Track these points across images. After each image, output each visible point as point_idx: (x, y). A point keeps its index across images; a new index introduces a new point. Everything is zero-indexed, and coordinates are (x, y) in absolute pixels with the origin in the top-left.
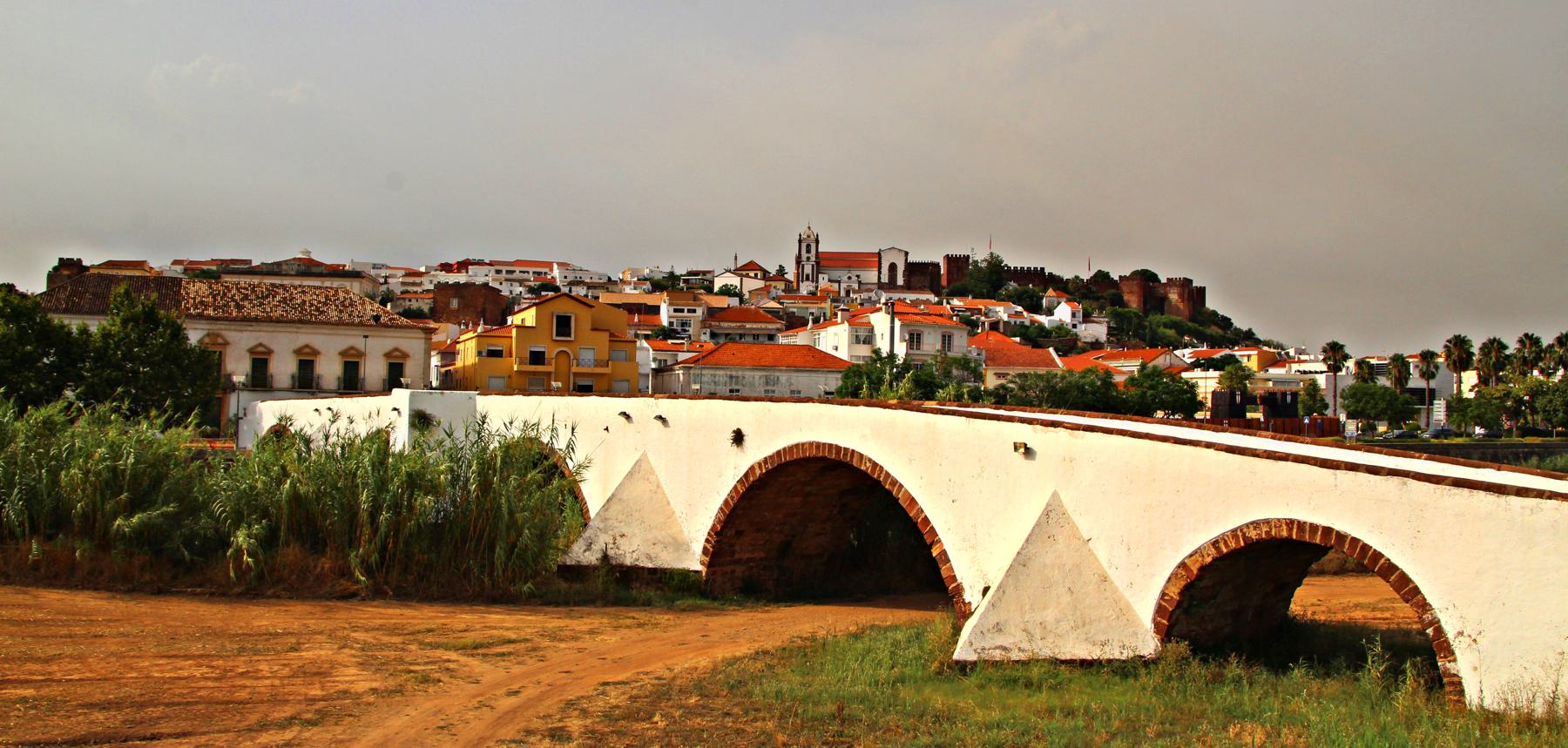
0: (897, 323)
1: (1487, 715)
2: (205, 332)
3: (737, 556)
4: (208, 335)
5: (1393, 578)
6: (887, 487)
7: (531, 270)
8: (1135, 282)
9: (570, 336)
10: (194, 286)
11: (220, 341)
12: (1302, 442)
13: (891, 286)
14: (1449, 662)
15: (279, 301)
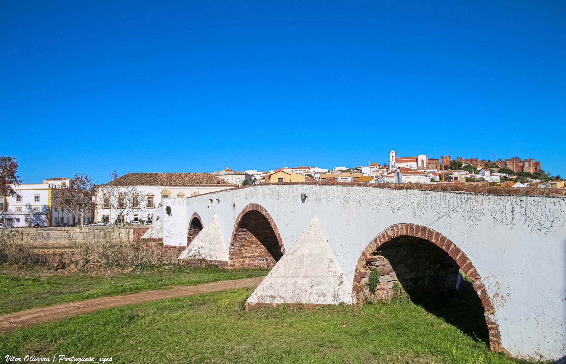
3: (244, 255)
6: (415, 236)
7: (303, 170)
8: (512, 161)
11: (168, 192)
14: (491, 314)
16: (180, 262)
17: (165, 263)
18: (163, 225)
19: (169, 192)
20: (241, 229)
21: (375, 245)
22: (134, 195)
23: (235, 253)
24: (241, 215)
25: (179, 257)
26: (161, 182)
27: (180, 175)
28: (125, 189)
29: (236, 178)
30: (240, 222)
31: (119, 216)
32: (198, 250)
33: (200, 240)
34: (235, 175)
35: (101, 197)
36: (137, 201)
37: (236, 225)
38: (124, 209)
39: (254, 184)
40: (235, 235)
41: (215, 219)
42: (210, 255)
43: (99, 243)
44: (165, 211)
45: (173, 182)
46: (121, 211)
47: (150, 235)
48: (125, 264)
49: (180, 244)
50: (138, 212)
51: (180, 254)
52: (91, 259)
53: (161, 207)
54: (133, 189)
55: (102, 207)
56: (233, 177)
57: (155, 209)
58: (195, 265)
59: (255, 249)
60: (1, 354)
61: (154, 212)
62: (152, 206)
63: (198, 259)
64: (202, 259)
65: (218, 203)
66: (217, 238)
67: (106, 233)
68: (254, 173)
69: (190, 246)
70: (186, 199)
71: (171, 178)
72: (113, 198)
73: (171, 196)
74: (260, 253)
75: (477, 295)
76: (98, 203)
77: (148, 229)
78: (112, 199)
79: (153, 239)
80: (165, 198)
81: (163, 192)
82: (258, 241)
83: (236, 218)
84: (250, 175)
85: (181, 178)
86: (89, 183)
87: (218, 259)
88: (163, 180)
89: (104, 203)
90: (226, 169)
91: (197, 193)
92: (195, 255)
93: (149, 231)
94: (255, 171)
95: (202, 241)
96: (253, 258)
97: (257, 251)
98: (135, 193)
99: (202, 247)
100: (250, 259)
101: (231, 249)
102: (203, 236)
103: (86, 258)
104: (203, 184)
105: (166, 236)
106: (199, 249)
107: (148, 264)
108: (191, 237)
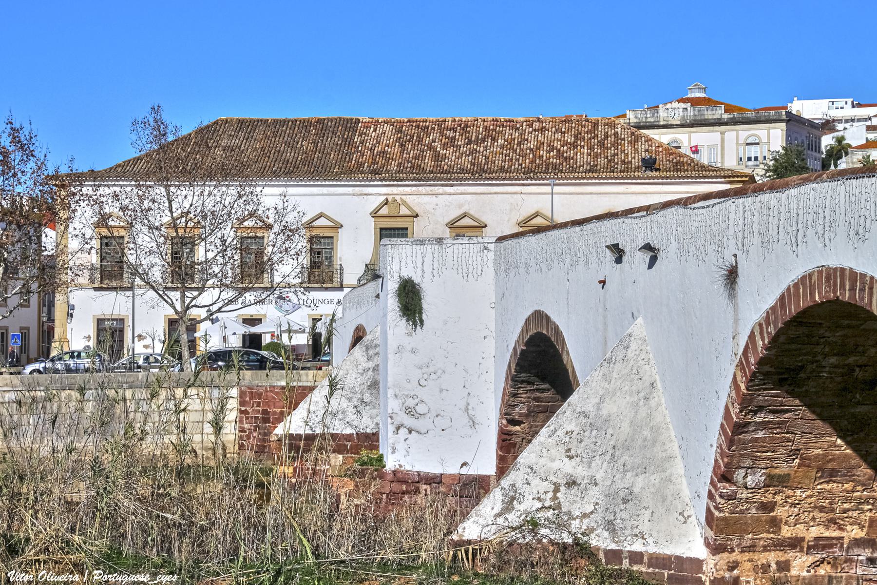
1: (188, 445)
3: (786, 532)
10: (375, 130)
11: (404, 211)
15: (502, 147)
16: (461, 554)
17: (391, 556)
18: (381, 367)
19: (409, 207)
20: (768, 395)
22: (246, 224)
23: (737, 521)
24: (768, 325)
25: (460, 530)
26: (374, 162)
27: (465, 128)
28: (202, 194)
29: (741, 141)
30: (761, 362)
31: (172, 323)
32: (550, 495)
33: (562, 449)
34: (735, 123)
35: (89, 233)
36: (260, 253)
37: (739, 374)
38: (195, 293)
39: (832, 168)
40: (740, 428)
41: (633, 346)
42: (610, 526)
43: (74, 456)
44: (392, 303)
45: (428, 162)
46: (183, 302)
47: (319, 418)
48: (197, 562)
49: (464, 464)
50: (264, 306)
51: (465, 515)
52: (32, 537)
53: (372, 284)
54: (240, 197)
55: (93, 282)
56: (723, 133)
57: (346, 290)
58: (539, 570)
59: (846, 506)
61: (340, 308)
62: (332, 281)
63: (551, 542)
64: (570, 541)
65: (650, 266)
66: (645, 440)
67: (107, 409)
68: (835, 114)
69: (514, 477)
70: (492, 247)
71: (420, 140)
72: (145, 239)
73: (420, 229)
74: (870, 526)
76: (71, 263)
77: (311, 389)
78: (139, 241)
79: (334, 436)
80: (395, 240)
81: (381, 212)
82: (856, 460)
83: (743, 341)
84: (810, 124)
85: (470, 142)
86: (31, 164)
87: (652, 549)
88: (383, 152)
89: (101, 261)
90: (689, 96)
91: (545, 218)
92: (534, 524)
93: (318, 397)
94: (840, 102)
95: (573, 452)
96: (837, 551)
97: (855, 514)
98: (251, 215)
99: (572, 483)
100: (818, 557)
101: (718, 500)
102: (577, 430)
103: (9, 527)
104: (574, 170)
105: (397, 422)
106: (557, 490)
107: (311, 560)
108: (515, 433)
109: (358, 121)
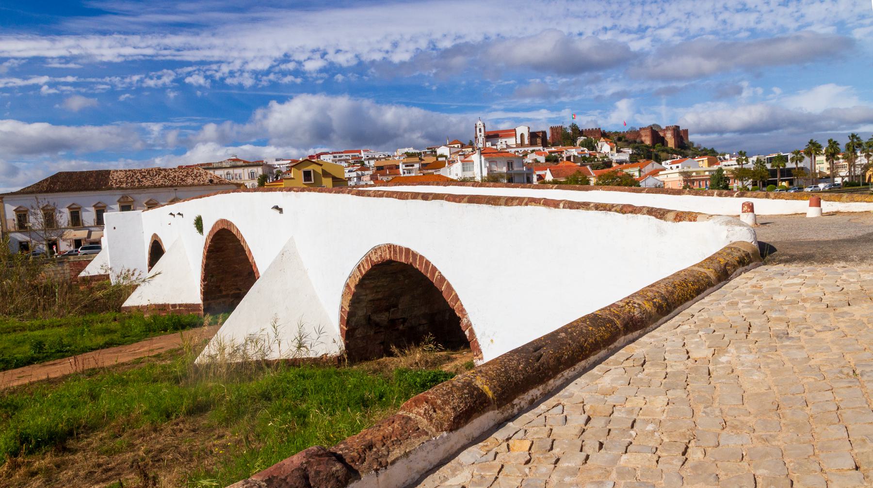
0: (483, 158)
2: (121, 196)
3: (224, 293)
4: (123, 197)
5: (443, 288)
7: (351, 154)
9: (311, 181)
12: (488, 187)
13: (522, 144)
15: (162, 177)
21: (358, 274)
45: (137, 184)
60: (280, 486)
75: (465, 336)
109: (110, 171)
